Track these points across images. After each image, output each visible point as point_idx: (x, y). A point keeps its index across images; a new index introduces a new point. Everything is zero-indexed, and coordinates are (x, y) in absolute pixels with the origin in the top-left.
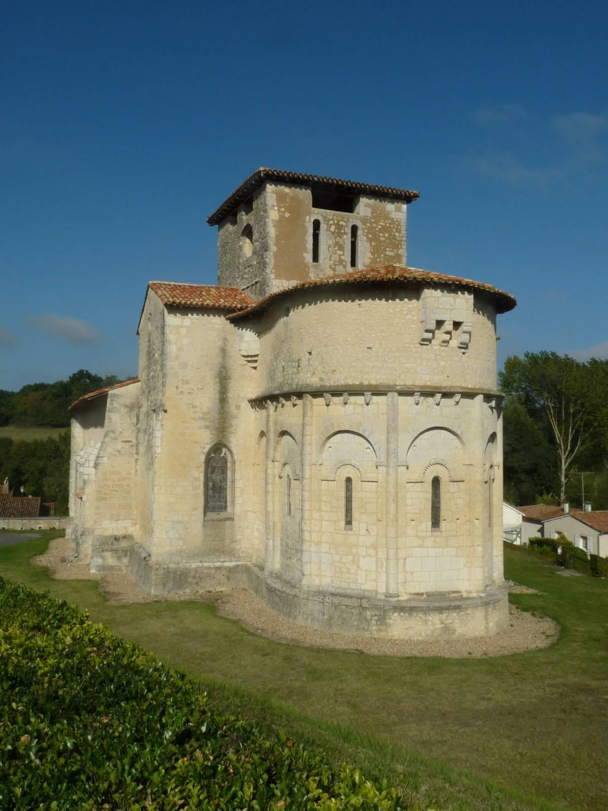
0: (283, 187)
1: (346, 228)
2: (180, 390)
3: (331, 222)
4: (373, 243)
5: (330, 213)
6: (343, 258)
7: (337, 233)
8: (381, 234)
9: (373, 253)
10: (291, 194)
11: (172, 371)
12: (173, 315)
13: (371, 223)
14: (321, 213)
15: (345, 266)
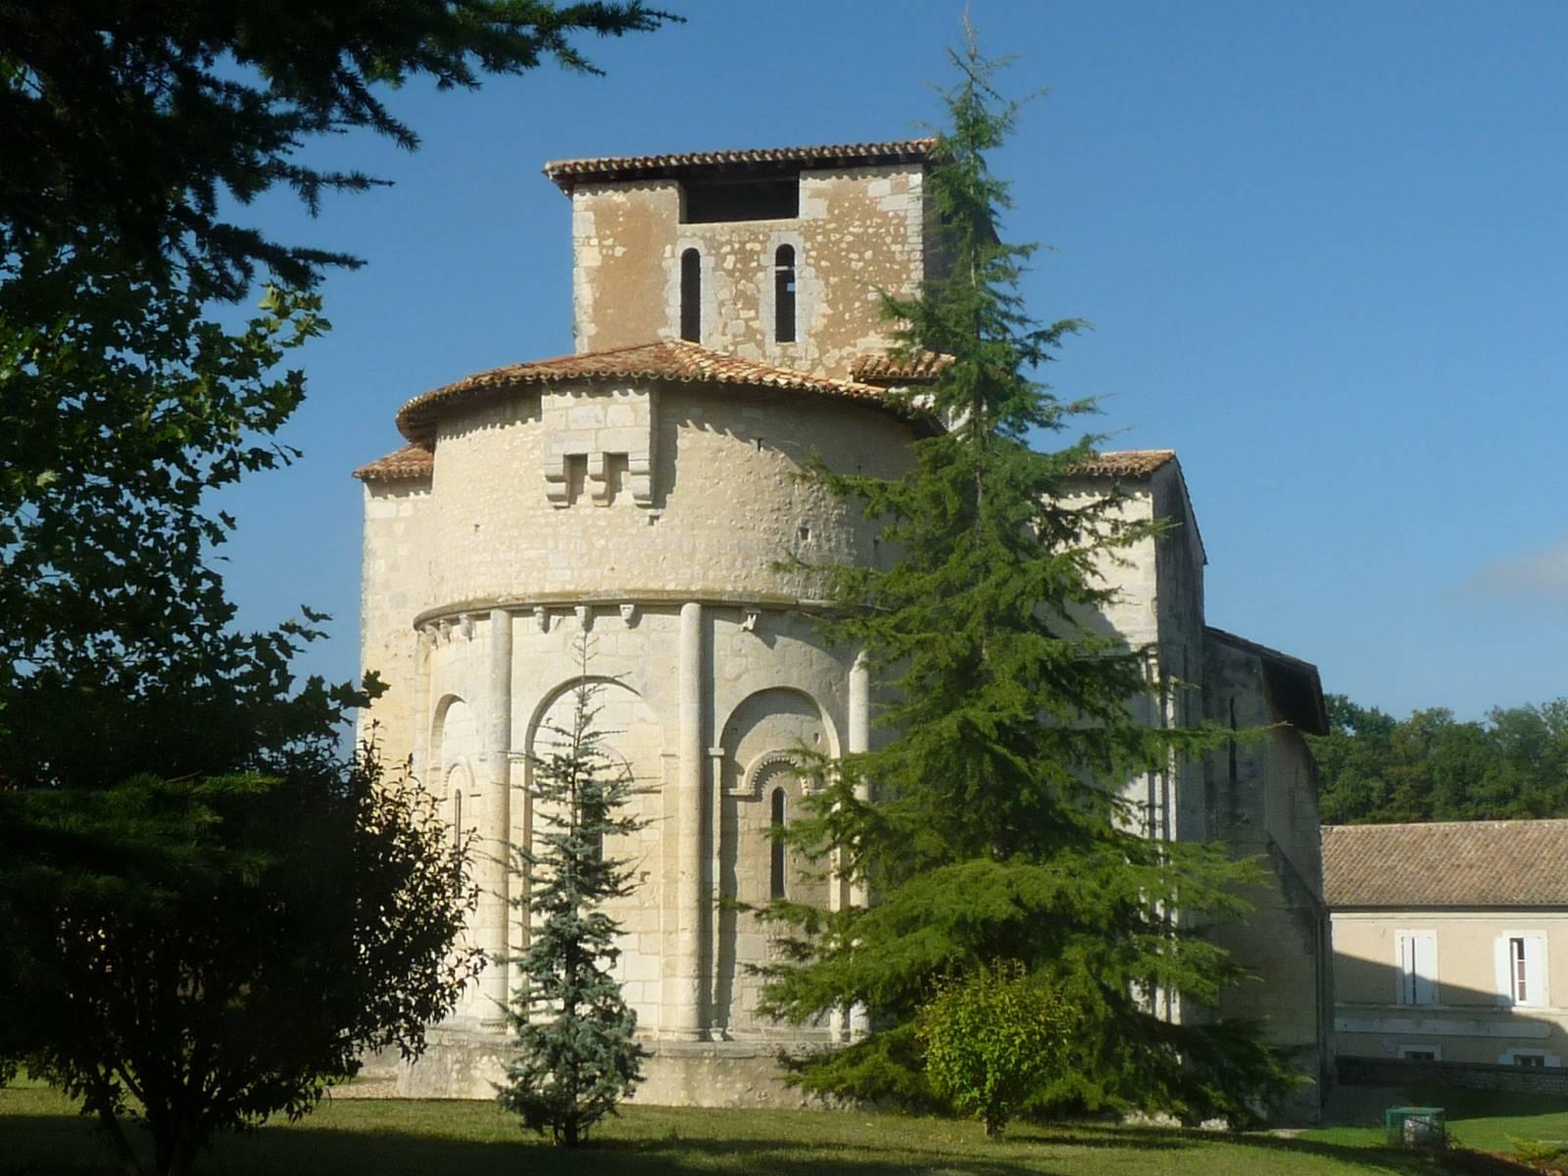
0: (610, 192)
1: (762, 256)
2: (392, 651)
3: (727, 249)
4: (833, 280)
5: (721, 229)
6: (755, 324)
7: (740, 271)
8: (854, 256)
9: (831, 303)
10: (629, 205)
11: (377, 613)
12: (381, 498)
13: (826, 233)
14: (699, 234)
15: (760, 344)
